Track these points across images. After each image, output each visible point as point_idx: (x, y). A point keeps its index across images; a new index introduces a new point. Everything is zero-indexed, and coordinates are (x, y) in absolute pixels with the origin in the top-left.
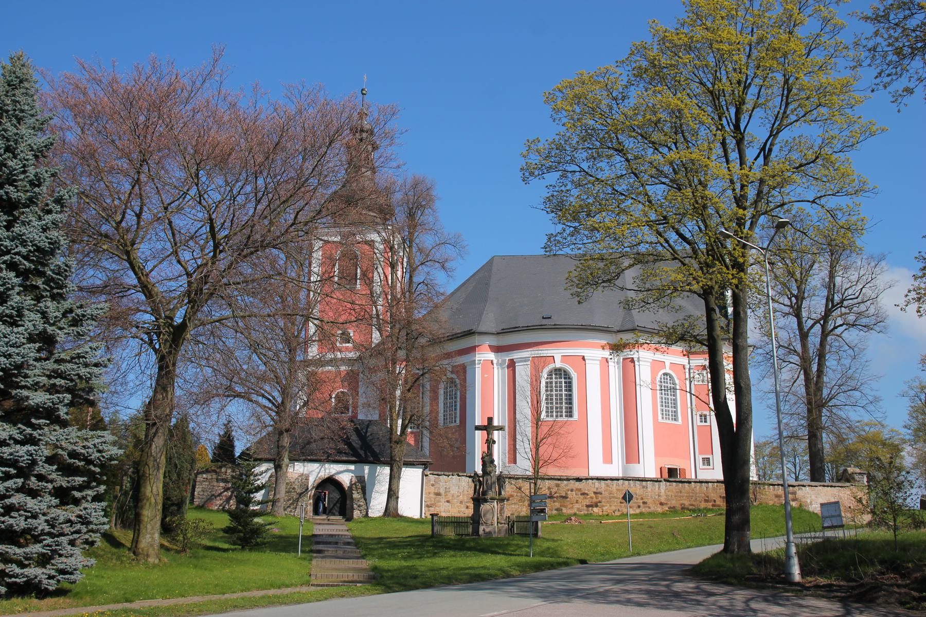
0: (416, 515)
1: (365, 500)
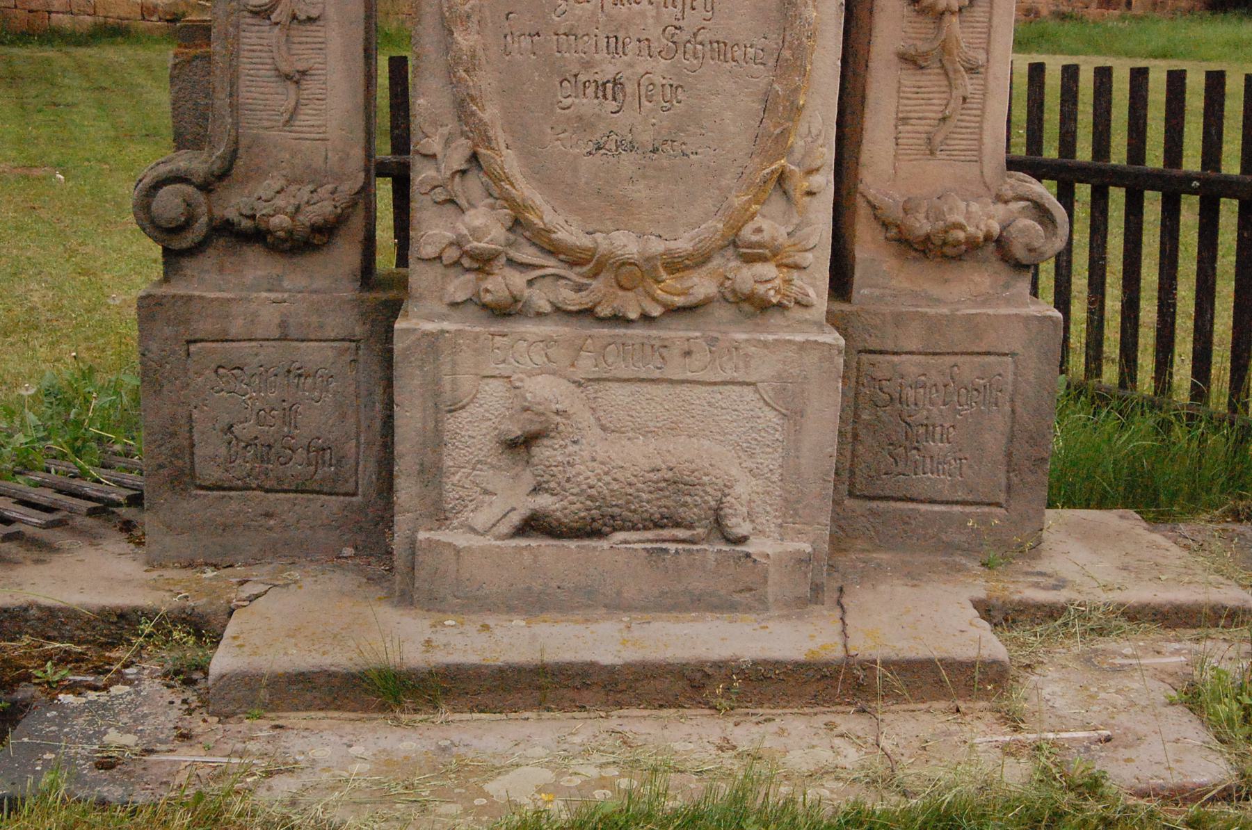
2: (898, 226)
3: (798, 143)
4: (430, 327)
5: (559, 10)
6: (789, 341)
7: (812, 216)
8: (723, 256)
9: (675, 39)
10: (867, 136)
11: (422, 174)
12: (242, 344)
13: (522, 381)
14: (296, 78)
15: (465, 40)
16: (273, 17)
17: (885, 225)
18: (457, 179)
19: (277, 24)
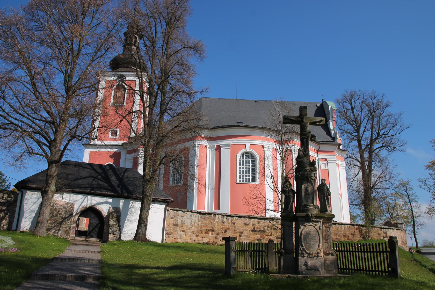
0: (159, 240)
1: (119, 226)
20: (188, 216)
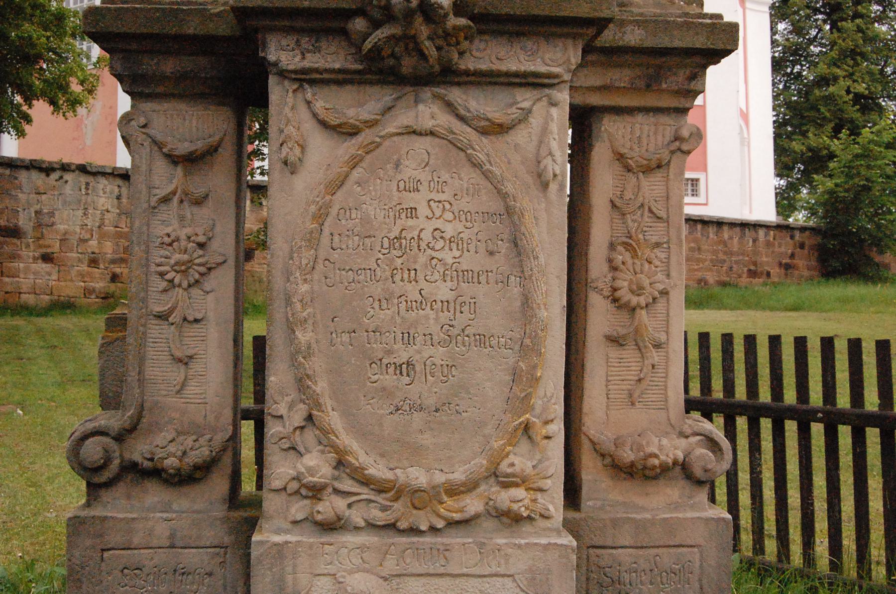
2: (611, 456)
3: (537, 403)
4: (277, 539)
5: (369, 315)
6: (536, 544)
7: (549, 453)
8: (487, 484)
9: (449, 333)
10: (587, 393)
11: (273, 429)
12: (142, 551)
13: (344, 577)
14: (185, 361)
15: (303, 337)
16: (170, 319)
17: (603, 456)
18: (298, 432)
19: (172, 324)
20: (68, 190)
